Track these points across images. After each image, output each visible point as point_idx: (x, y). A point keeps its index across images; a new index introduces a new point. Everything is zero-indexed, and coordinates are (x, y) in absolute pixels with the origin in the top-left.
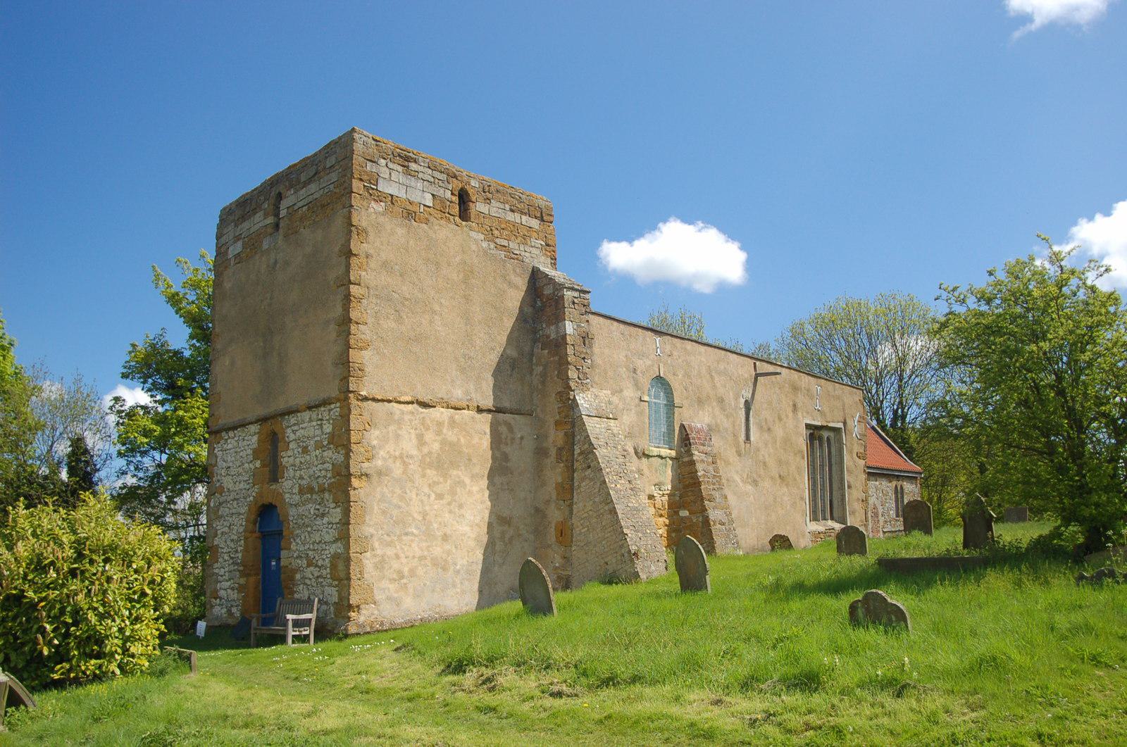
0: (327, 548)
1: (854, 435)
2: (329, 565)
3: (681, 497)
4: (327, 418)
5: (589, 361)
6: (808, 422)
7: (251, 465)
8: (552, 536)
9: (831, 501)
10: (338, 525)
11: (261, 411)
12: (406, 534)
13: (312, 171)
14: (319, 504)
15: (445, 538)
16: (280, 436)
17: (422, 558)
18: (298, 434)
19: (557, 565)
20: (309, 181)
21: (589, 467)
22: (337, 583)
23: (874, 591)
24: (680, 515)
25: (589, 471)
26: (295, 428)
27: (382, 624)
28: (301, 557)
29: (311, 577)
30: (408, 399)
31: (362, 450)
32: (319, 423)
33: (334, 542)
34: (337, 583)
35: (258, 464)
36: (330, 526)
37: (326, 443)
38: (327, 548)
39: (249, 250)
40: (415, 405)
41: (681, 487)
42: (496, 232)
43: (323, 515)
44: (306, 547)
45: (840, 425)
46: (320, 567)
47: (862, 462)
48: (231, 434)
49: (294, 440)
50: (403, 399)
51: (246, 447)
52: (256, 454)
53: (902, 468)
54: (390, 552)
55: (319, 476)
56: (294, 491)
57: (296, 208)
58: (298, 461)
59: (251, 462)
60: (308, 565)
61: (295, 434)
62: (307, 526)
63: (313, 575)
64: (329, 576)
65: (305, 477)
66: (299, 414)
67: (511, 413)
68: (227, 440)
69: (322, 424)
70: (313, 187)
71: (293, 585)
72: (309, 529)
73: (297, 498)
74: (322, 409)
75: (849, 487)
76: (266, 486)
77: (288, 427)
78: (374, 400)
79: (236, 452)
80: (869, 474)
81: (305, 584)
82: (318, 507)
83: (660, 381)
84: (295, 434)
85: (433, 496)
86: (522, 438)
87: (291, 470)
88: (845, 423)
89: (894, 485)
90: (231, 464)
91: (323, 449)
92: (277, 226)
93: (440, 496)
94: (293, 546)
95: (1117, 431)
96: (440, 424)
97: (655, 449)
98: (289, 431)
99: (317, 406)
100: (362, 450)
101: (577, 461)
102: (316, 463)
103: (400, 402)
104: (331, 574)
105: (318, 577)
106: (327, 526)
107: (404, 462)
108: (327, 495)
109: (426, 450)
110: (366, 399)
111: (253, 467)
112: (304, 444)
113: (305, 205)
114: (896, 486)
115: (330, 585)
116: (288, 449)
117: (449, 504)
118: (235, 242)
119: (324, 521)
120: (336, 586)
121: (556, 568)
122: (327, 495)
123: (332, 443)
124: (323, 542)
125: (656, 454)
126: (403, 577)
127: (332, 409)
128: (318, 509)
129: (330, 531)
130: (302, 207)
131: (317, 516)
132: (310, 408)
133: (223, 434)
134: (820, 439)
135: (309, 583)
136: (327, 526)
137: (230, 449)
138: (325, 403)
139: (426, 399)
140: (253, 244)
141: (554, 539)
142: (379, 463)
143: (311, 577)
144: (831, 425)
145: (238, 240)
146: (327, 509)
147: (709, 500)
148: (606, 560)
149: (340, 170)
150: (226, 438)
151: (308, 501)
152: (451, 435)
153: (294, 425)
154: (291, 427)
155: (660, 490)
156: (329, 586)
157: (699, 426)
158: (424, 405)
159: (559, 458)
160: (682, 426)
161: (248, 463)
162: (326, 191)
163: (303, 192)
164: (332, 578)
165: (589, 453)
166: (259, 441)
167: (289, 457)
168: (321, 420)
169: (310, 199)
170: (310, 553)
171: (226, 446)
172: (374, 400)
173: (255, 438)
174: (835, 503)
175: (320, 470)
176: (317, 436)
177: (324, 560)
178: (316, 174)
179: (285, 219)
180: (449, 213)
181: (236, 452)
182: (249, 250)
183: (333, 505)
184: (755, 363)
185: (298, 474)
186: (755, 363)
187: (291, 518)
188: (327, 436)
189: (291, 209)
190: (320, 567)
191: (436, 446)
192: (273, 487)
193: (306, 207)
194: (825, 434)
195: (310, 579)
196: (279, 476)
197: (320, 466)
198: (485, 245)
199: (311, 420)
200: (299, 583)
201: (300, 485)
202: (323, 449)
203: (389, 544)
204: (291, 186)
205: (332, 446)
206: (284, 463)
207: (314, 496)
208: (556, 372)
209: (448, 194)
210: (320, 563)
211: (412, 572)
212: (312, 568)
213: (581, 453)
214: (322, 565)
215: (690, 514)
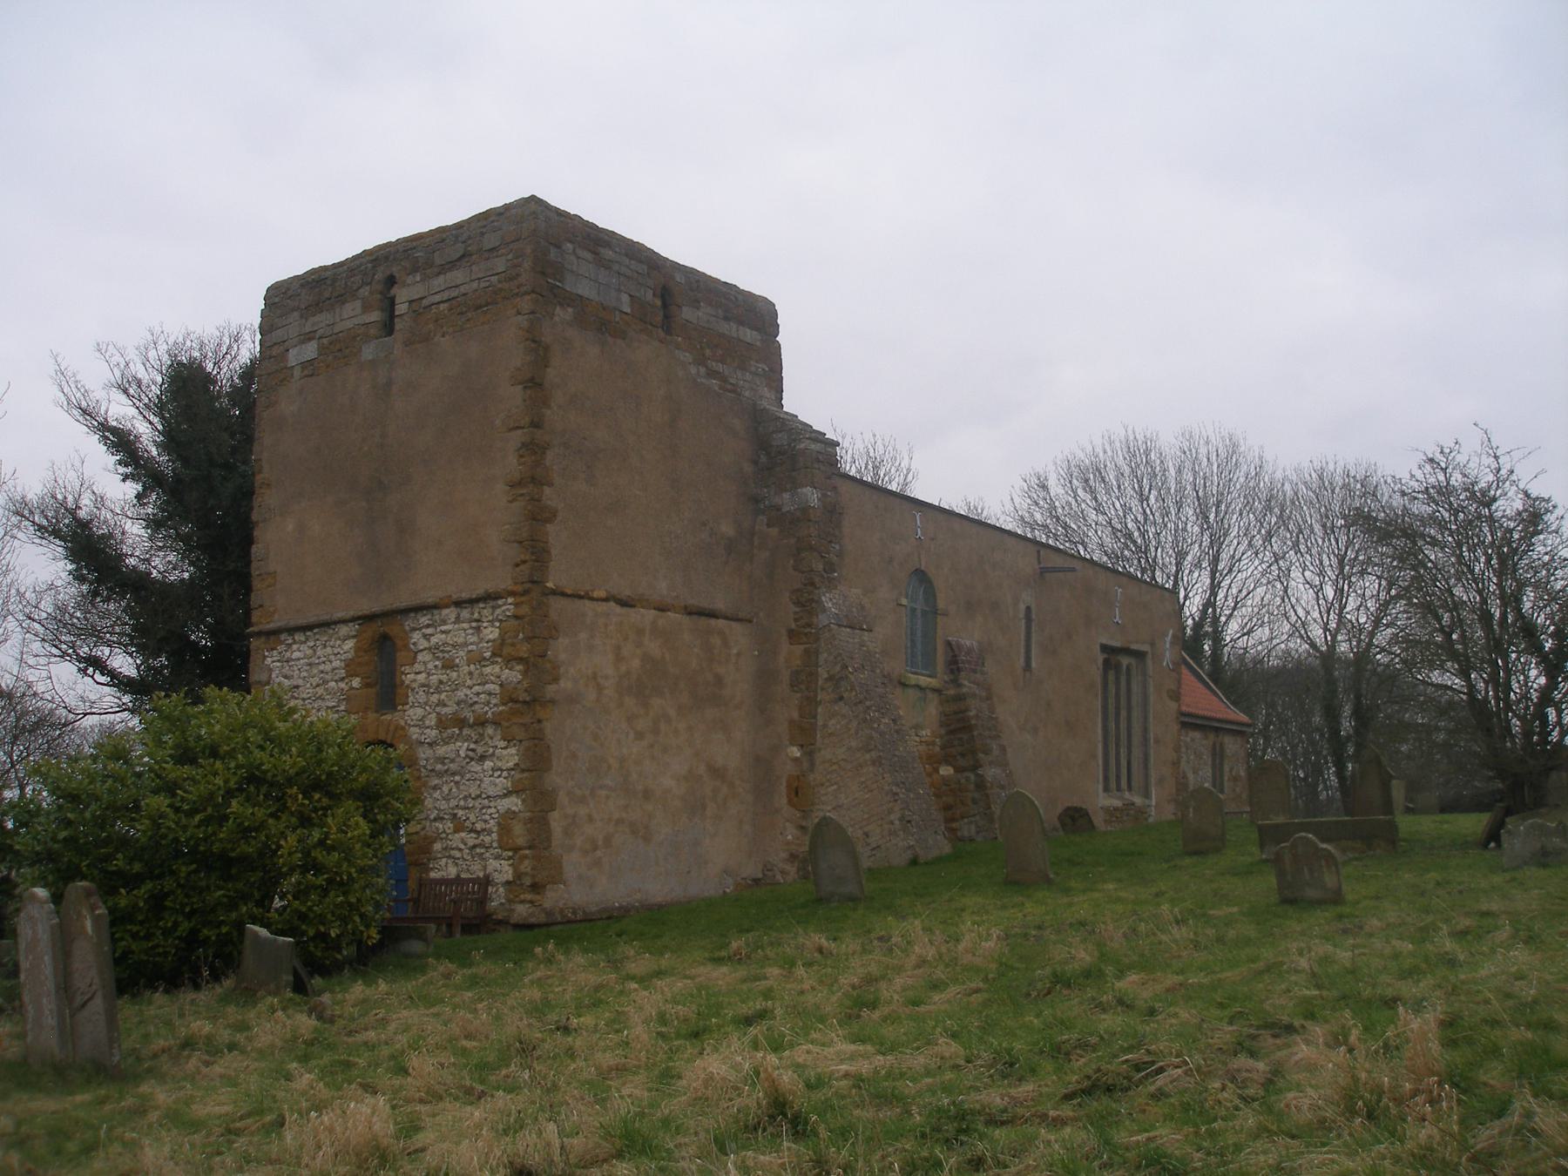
0: (492, 804)
1: (1165, 664)
2: (495, 829)
3: (943, 748)
4: (491, 618)
5: (837, 547)
6: (1104, 642)
7: (342, 685)
8: (781, 800)
9: (1129, 763)
10: (513, 772)
11: (367, 606)
12: (601, 787)
13: (459, 249)
14: (476, 742)
15: (647, 794)
16: (399, 643)
17: (619, 822)
18: (434, 640)
19: (790, 837)
20: (452, 265)
21: (841, 698)
22: (510, 854)
23: (1303, 834)
24: (941, 773)
25: (841, 703)
26: (429, 631)
27: (574, 913)
28: (442, 819)
29: (463, 847)
30: (602, 594)
31: (548, 665)
32: (474, 624)
33: (505, 796)
34: (510, 854)
35: (356, 682)
36: (496, 774)
37: (488, 654)
38: (492, 804)
39: (330, 357)
40: (612, 604)
41: (943, 732)
42: (708, 352)
43: (482, 758)
44: (453, 803)
45: (1145, 648)
46: (478, 833)
47: (1173, 705)
48: (299, 637)
49: (425, 649)
50: (595, 595)
51: (332, 657)
52: (351, 668)
53: (1219, 716)
54: (583, 811)
55: (476, 703)
56: (427, 723)
57: (425, 302)
58: (434, 679)
59: (342, 679)
60: (456, 831)
61: (429, 640)
62: (454, 774)
63: (465, 844)
64: (495, 845)
65: (449, 703)
66: (435, 612)
67: (726, 618)
68: (290, 645)
69: (479, 627)
70: (457, 276)
71: (429, 860)
72: (457, 778)
73: (433, 734)
74: (481, 605)
75: (1157, 741)
76: (372, 716)
77: (414, 629)
78: (564, 594)
79: (310, 665)
80: (1184, 725)
81: (449, 857)
82: (472, 746)
83: (921, 576)
84: (429, 640)
85: (632, 735)
86: (739, 655)
87: (421, 693)
88: (1153, 645)
89: (1211, 743)
90: (300, 682)
91: (483, 663)
92: (388, 327)
93: (640, 736)
94: (428, 803)
95: (1552, 670)
96: (640, 632)
97: (912, 676)
98: (416, 636)
99: (472, 602)
100: (548, 665)
101: (822, 689)
102: (469, 682)
103: (592, 599)
104: (499, 841)
105: (475, 846)
106: (491, 773)
107: (598, 685)
108: (490, 730)
109: (623, 669)
110: (554, 592)
111: (346, 688)
112: (447, 655)
113: (446, 301)
114: (1214, 744)
115: (497, 857)
116: (414, 661)
117: (652, 746)
118: (302, 342)
119: (485, 767)
120: (510, 858)
121: (788, 843)
122: (490, 730)
123: (501, 656)
124: (484, 796)
125: (913, 683)
126: (595, 848)
127: (500, 606)
128: (473, 750)
129: (497, 780)
130: (438, 303)
131: (472, 759)
132: (459, 604)
133: (283, 637)
134: (1118, 667)
135: (457, 854)
136: (491, 773)
137: (299, 659)
138: (489, 598)
139: (626, 592)
140: (339, 349)
141: (784, 801)
142: (569, 685)
143: (463, 847)
144: (1134, 647)
145: (310, 339)
146: (491, 750)
147: (983, 752)
148: (866, 829)
149: (510, 257)
150: (290, 641)
151: (458, 737)
152: (654, 647)
153: (428, 626)
154: (420, 629)
155: (917, 735)
156: (496, 858)
157: (968, 643)
158: (623, 603)
159: (794, 685)
160: (949, 644)
161: (336, 681)
162: (483, 285)
163: (439, 282)
164: (501, 848)
165: (841, 678)
166: (357, 649)
167: (417, 673)
168: (478, 621)
169: (454, 293)
170: (460, 813)
171: (288, 654)
172: (564, 594)
173: (350, 644)
174: (1135, 765)
175: (478, 694)
176: (471, 644)
177: (486, 821)
178: (463, 256)
179: (405, 318)
180: (651, 324)
181: (310, 665)
182: (330, 357)
183: (503, 744)
184: (1038, 552)
185: (435, 698)
186: (1038, 552)
187: (423, 763)
188: (490, 644)
189: (414, 304)
190: (478, 833)
191: (636, 663)
192: (388, 717)
193: (446, 305)
194: (1125, 661)
195: (460, 850)
196: (397, 701)
197: (477, 687)
198: (693, 370)
199: (458, 620)
200: (439, 855)
201: (438, 714)
202: (483, 663)
203: (582, 800)
204: (415, 270)
205: (499, 660)
206: (407, 682)
207: (466, 731)
208: (792, 562)
209: (649, 296)
210: (479, 826)
211: (608, 840)
212: (463, 834)
213: (831, 678)
214: (484, 830)
215: (955, 771)
